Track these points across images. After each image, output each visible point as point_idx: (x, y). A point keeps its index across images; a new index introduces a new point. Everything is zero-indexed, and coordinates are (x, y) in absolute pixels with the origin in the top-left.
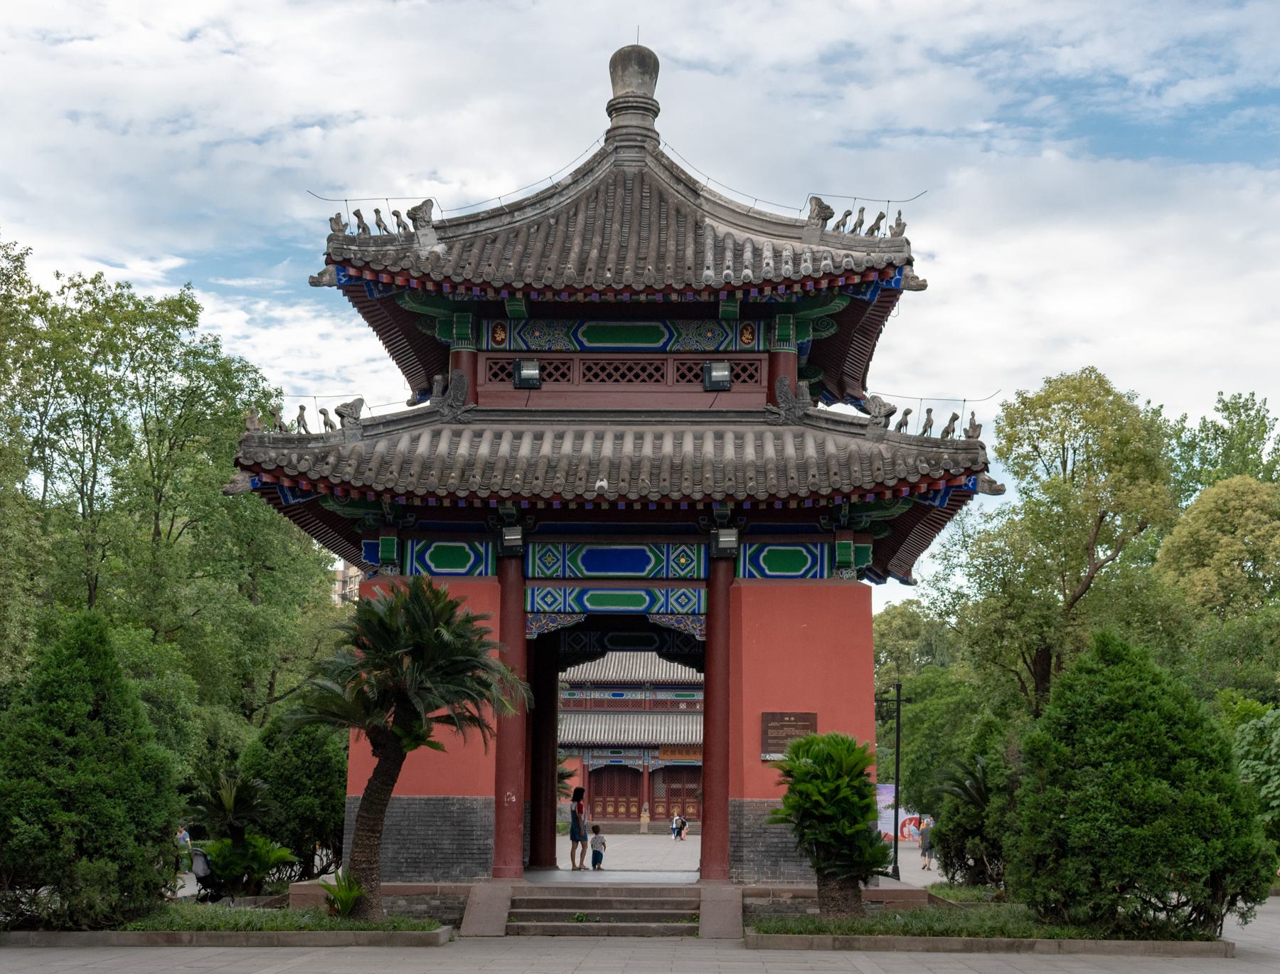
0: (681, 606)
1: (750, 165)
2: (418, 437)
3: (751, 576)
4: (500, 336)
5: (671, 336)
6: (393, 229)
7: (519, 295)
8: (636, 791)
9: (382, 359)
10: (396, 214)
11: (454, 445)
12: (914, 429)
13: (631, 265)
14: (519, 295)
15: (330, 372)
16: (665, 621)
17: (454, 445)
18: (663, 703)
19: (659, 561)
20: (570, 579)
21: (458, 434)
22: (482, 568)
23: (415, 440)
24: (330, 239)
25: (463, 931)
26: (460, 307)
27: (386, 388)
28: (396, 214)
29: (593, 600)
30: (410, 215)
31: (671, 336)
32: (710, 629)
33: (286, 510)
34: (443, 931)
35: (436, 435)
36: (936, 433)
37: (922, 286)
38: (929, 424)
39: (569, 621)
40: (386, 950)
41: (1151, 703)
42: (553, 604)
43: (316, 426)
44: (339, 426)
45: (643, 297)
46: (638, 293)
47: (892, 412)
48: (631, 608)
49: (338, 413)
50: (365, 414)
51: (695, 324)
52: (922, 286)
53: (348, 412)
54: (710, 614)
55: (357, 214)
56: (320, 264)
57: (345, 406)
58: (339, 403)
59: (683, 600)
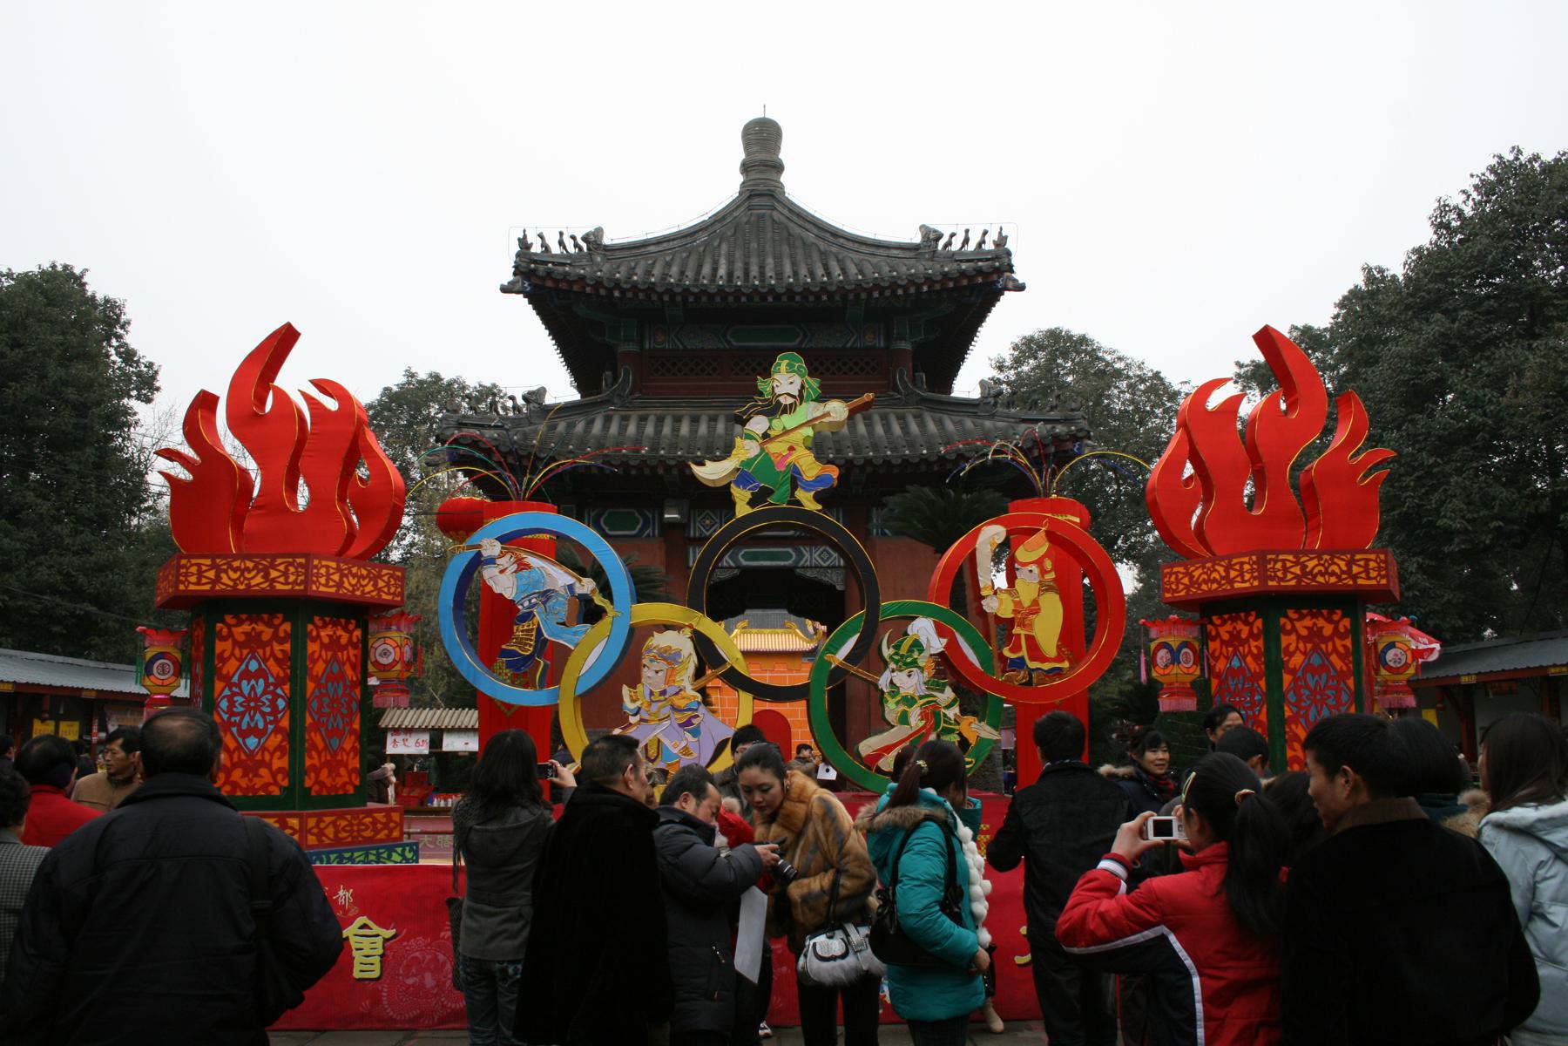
1: (865, 192)
4: (660, 338)
5: (805, 336)
6: (572, 250)
10: (573, 238)
11: (623, 429)
12: (956, 246)
13: (781, 271)
15: (525, 362)
16: (809, 574)
17: (623, 429)
21: (626, 419)
22: (649, 531)
23: (590, 423)
27: (562, 388)
28: (573, 238)
29: (789, 556)
30: (585, 239)
31: (805, 336)
36: (971, 247)
37: (1021, 288)
38: (966, 241)
47: (940, 236)
48: (782, 563)
50: (549, 400)
52: (1021, 288)
53: (593, 239)
55: (541, 236)
56: (508, 276)
57: (530, 393)
58: (525, 390)
59: (825, 556)
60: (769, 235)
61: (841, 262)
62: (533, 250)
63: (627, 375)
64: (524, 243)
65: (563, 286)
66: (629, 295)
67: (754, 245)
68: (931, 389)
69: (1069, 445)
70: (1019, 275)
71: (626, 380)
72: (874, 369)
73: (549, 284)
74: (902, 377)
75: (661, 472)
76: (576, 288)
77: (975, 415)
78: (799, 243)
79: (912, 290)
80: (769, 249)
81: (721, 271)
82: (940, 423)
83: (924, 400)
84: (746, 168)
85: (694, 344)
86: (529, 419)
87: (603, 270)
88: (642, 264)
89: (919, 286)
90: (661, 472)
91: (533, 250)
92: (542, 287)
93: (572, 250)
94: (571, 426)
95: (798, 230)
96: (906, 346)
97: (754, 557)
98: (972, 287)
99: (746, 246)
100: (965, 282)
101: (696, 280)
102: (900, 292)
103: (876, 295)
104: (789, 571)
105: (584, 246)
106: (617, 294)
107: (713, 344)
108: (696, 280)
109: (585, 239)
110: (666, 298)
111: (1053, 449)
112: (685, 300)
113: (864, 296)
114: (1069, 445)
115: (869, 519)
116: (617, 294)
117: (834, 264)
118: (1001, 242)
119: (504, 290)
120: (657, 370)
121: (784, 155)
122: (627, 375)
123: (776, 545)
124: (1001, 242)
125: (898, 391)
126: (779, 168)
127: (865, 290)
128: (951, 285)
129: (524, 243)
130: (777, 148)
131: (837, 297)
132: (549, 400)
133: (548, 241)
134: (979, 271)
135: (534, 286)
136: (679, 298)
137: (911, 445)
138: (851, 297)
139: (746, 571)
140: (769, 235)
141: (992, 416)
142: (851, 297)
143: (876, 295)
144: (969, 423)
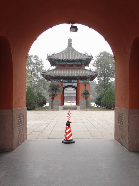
0: (75, 85)
13: (71, 57)
16: (74, 86)
32: (77, 86)
41: (86, 96)
42: (65, 85)
54: (77, 85)
56: (46, 58)
64: (48, 55)
121: (72, 42)
129: (48, 55)
139: (68, 85)
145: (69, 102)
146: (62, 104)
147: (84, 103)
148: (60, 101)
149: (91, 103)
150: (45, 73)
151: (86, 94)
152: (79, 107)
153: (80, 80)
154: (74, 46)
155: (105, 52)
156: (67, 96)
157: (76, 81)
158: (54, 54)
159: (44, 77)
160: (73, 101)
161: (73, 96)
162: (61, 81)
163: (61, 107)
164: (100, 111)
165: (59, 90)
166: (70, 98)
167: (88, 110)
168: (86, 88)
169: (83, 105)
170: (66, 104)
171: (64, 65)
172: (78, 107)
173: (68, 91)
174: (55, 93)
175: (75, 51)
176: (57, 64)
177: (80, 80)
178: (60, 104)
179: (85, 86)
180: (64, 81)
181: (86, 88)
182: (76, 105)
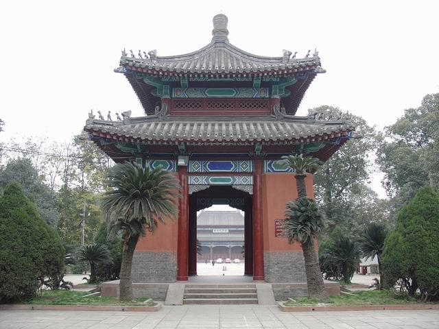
0: (243, 183)
2: (150, 125)
3: (269, 171)
7: (182, 143)
8: (227, 253)
9: (188, 309)
13: (223, 64)
14: (182, 143)
16: (238, 188)
18: (209, 231)
19: (236, 166)
20: (204, 173)
24: (122, 58)
25: (166, 302)
26: (166, 83)
27: (138, 111)
29: (212, 180)
32: (255, 190)
33: (102, 147)
34: (159, 303)
35: (157, 124)
37: (324, 72)
39: (204, 188)
40: (176, 239)
41: (309, 232)
42: (199, 183)
43: (114, 119)
44: (122, 119)
45: (206, 144)
46: (204, 142)
49: (122, 114)
51: (245, 89)
54: (255, 185)
56: (117, 66)
59: (245, 180)
60: (223, 56)
61: (244, 63)
62: (128, 56)
63: (165, 107)
64: (124, 53)
65: (139, 70)
66: (166, 74)
67: (217, 60)
68: (288, 113)
69: (346, 133)
70: (324, 66)
71: (164, 109)
72: (264, 106)
73: (134, 69)
74: (276, 107)
75: (177, 143)
76: (144, 71)
77: (306, 123)
78: (235, 59)
79: (280, 73)
80: (223, 61)
81: (203, 66)
82: (292, 126)
83: (285, 118)
84: (214, 32)
85: (192, 95)
86: (124, 123)
87: (155, 64)
88: (193, 62)
89: (283, 71)
90: (177, 143)
91: (128, 56)
92: (131, 71)
93: (144, 57)
94: (141, 126)
95: (234, 55)
96: (277, 97)
97: (215, 180)
98: (304, 72)
99: (214, 60)
100: (302, 70)
101: (207, 68)
102: (275, 73)
103: (266, 74)
104: (229, 187)
105: (149, 56)
106: (161, 73)
107: (199, 95)
108: (207, 68)
109: (149, 54)
110: (181, 75)
111: (340, 135)
112: (188, 76)
113: (261, 75)
114: (346, 133)
115: (263, 167)
116: (161, 73)
117: (241, 63)
118: (316, 54)
119: (116, 71)
120: (177, 106)
121: (229, 28)
122: (165, 107)
123: (224, 175)
124: (316, 54)
125: (274, 114)
126: (227, 32)
127: (261, 72)
128: (296, 70)
129: (124, 53)
130: (226, 25)
131: (250, 76)
132: (133, 116)
133: (134, 53)
134: (307, 66)
135: (128, 70)
136: (186, 75)
137: (281, 133)
138: (256, 75)
139: (212, 187)
140: (223, 56)
141: (313, 123)
142: (256, 75)
143: (266, 74)
144: (304, 125)
145: (218, 261)
146: (188, 269)
147: (288, 268)
148: (173, 259)
149: (363, 260)
150: (106, 127)
151: (308, 219)
152: (264, 288)
153: (266, 163)
154: (234, 39)
155: (333, 112)
156: (213, 246)
157: (248, 166)
158: (153, 56)
159: (103, 143)
160: (237, 260)
161: (228, 246)
162: (180, 168)
163: (177, 288)
164: (386, 312)
165: (158, 198)
166: (221, 251)
167: (321, 309)
168: (302, 192)
169: (281, 279)
170: (204, 269)
171: (201, 100)
172: (260, 285)
173: (216, 236)
174: (136, 214)
175: (243, 53)
176: (168, 97)
177: (266, 163)
178: (175, 274)
179: (297, 177)
180: (196, 167)
181: (302, 192)
182: (249, 271)
